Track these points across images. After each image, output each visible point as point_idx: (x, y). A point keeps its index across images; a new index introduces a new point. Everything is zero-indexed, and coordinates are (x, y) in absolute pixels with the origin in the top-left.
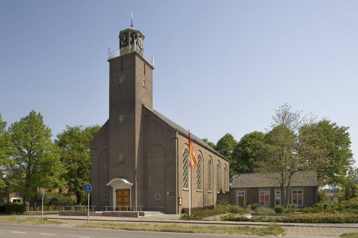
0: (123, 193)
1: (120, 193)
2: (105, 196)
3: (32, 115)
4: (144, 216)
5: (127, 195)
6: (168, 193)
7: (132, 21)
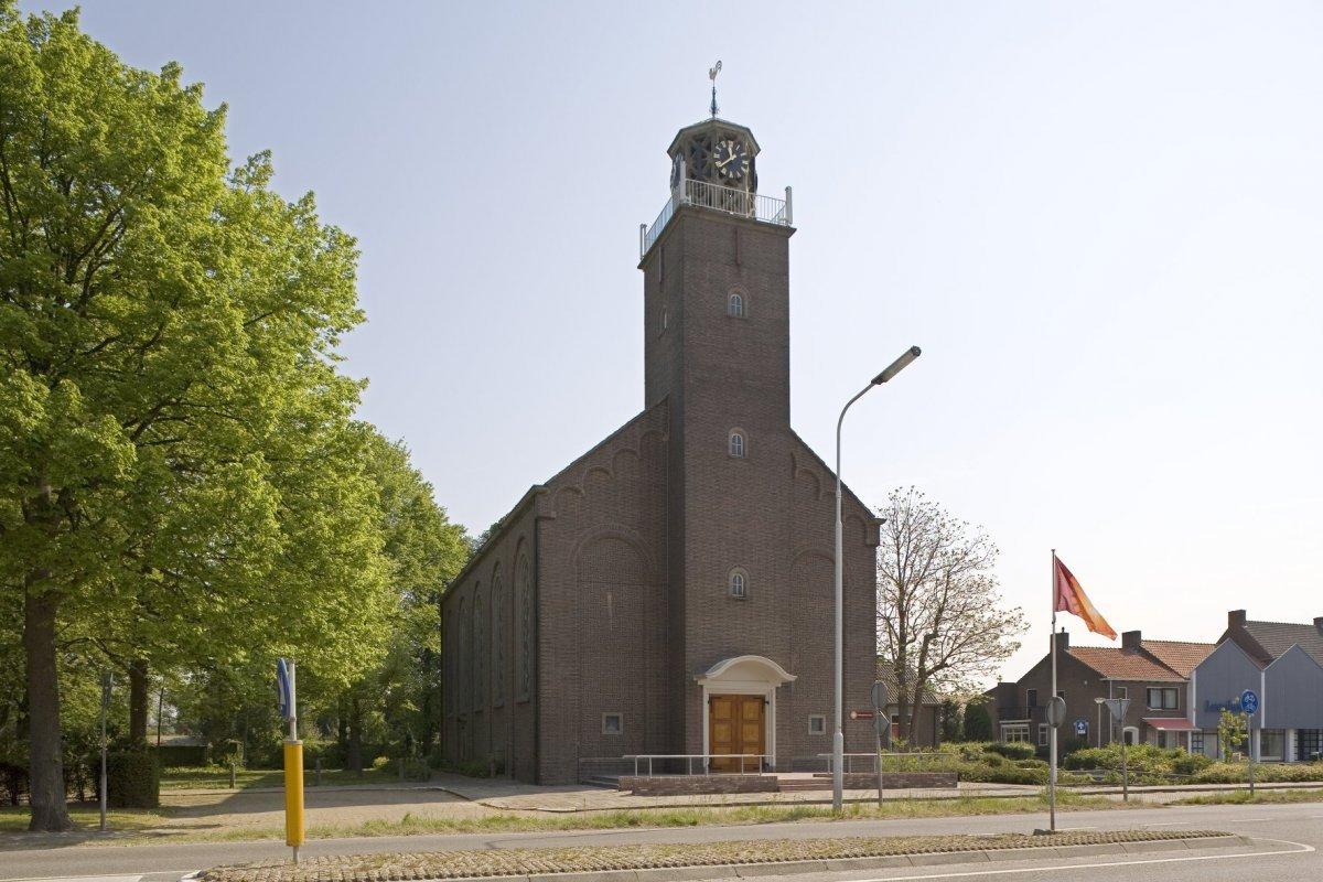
0: (740, 711)
1: (724, 709)
2: (618, 717)
3: (173, 65)
4: (108, 807)
5: (751, 716)
6: (854, 715)
7: (714, 94)
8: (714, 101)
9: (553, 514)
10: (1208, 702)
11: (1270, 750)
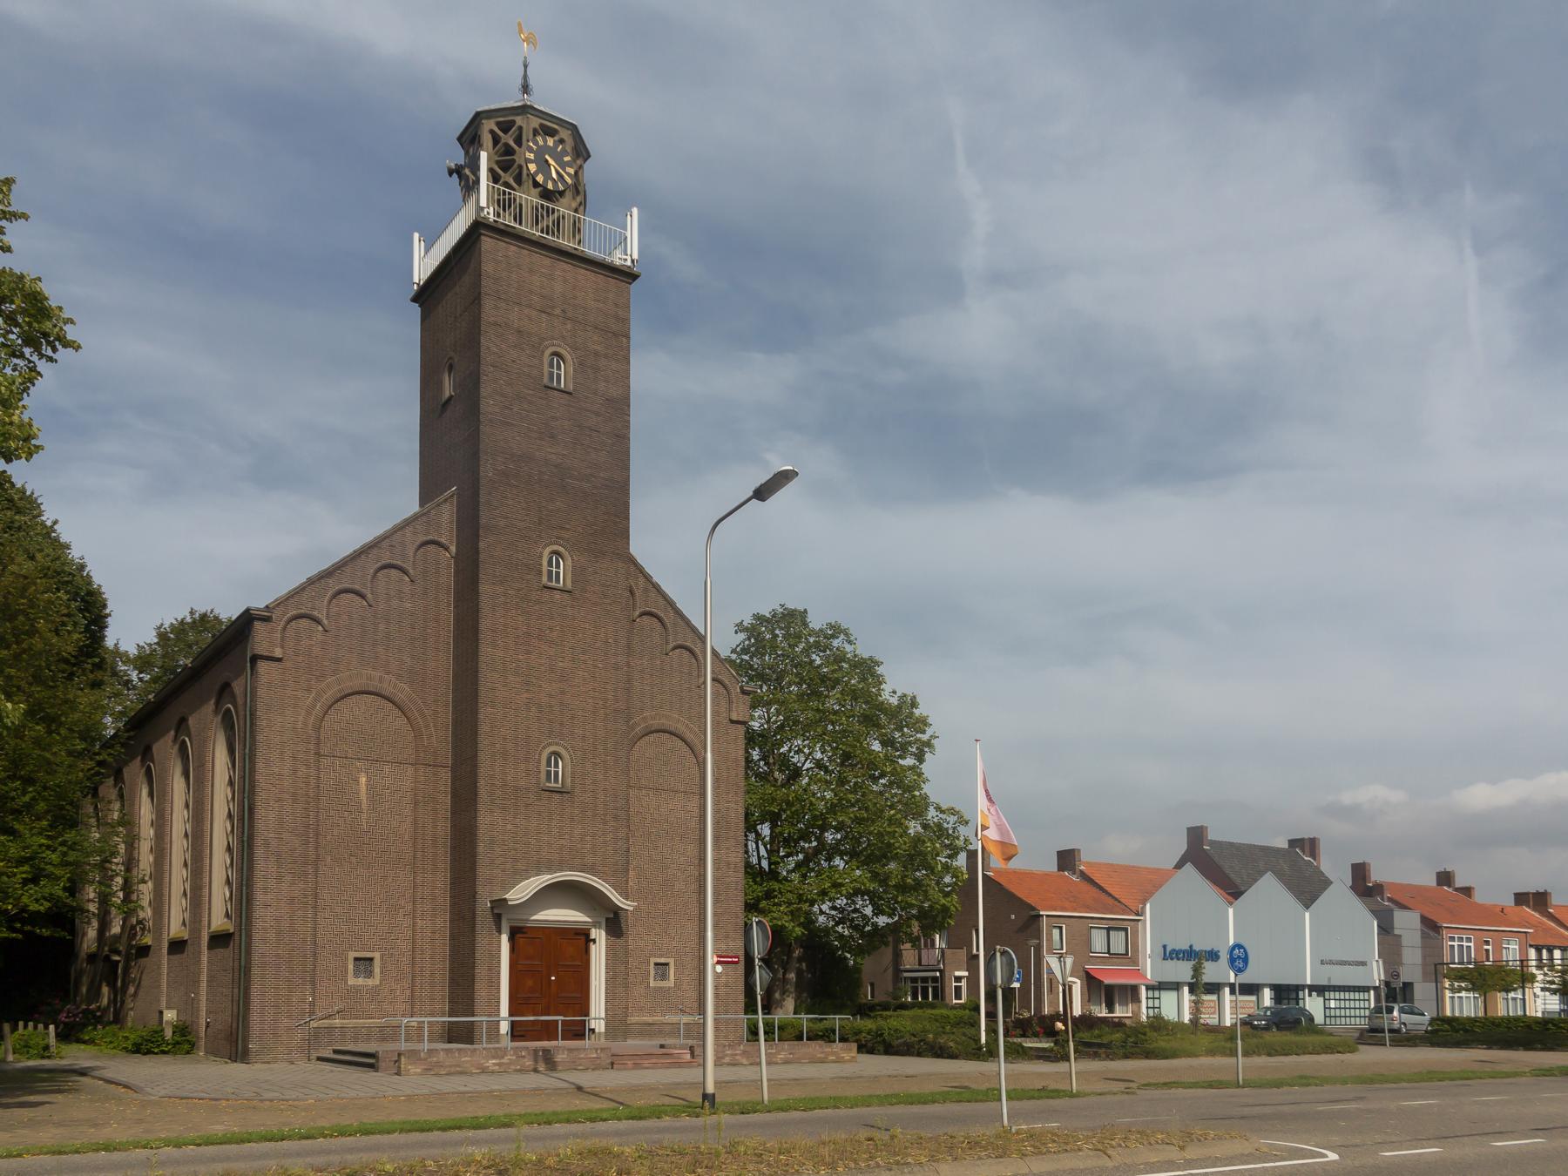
8: (525, 77)
9: (278, 653)
10: (42, 377)
11: (773, 1010)
